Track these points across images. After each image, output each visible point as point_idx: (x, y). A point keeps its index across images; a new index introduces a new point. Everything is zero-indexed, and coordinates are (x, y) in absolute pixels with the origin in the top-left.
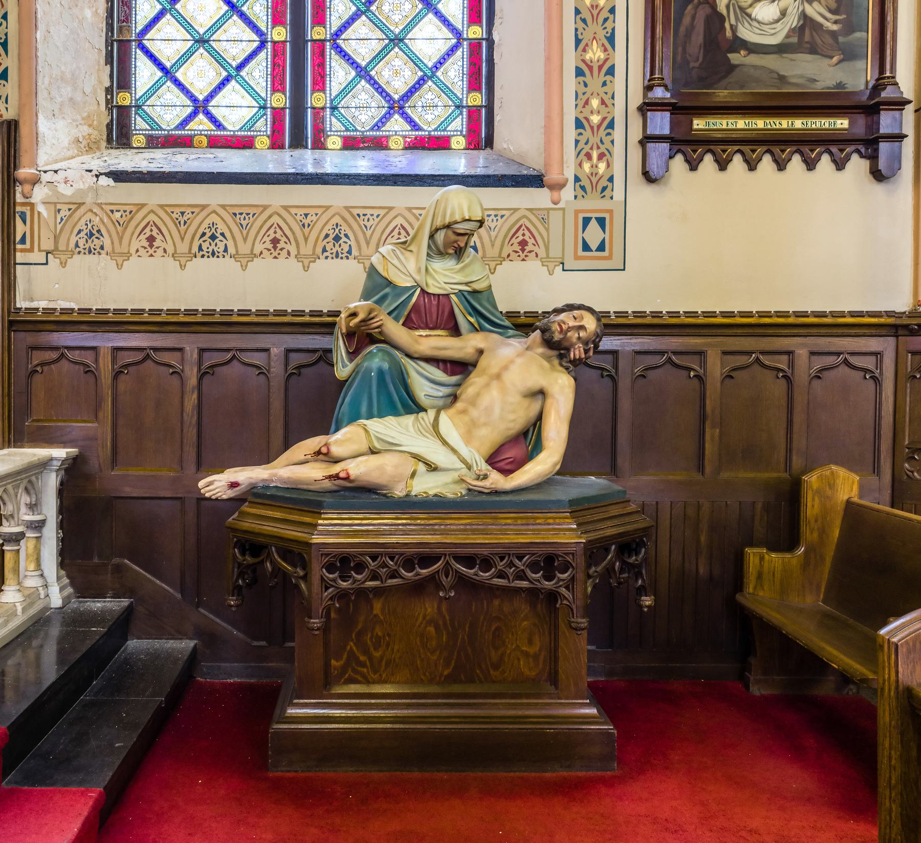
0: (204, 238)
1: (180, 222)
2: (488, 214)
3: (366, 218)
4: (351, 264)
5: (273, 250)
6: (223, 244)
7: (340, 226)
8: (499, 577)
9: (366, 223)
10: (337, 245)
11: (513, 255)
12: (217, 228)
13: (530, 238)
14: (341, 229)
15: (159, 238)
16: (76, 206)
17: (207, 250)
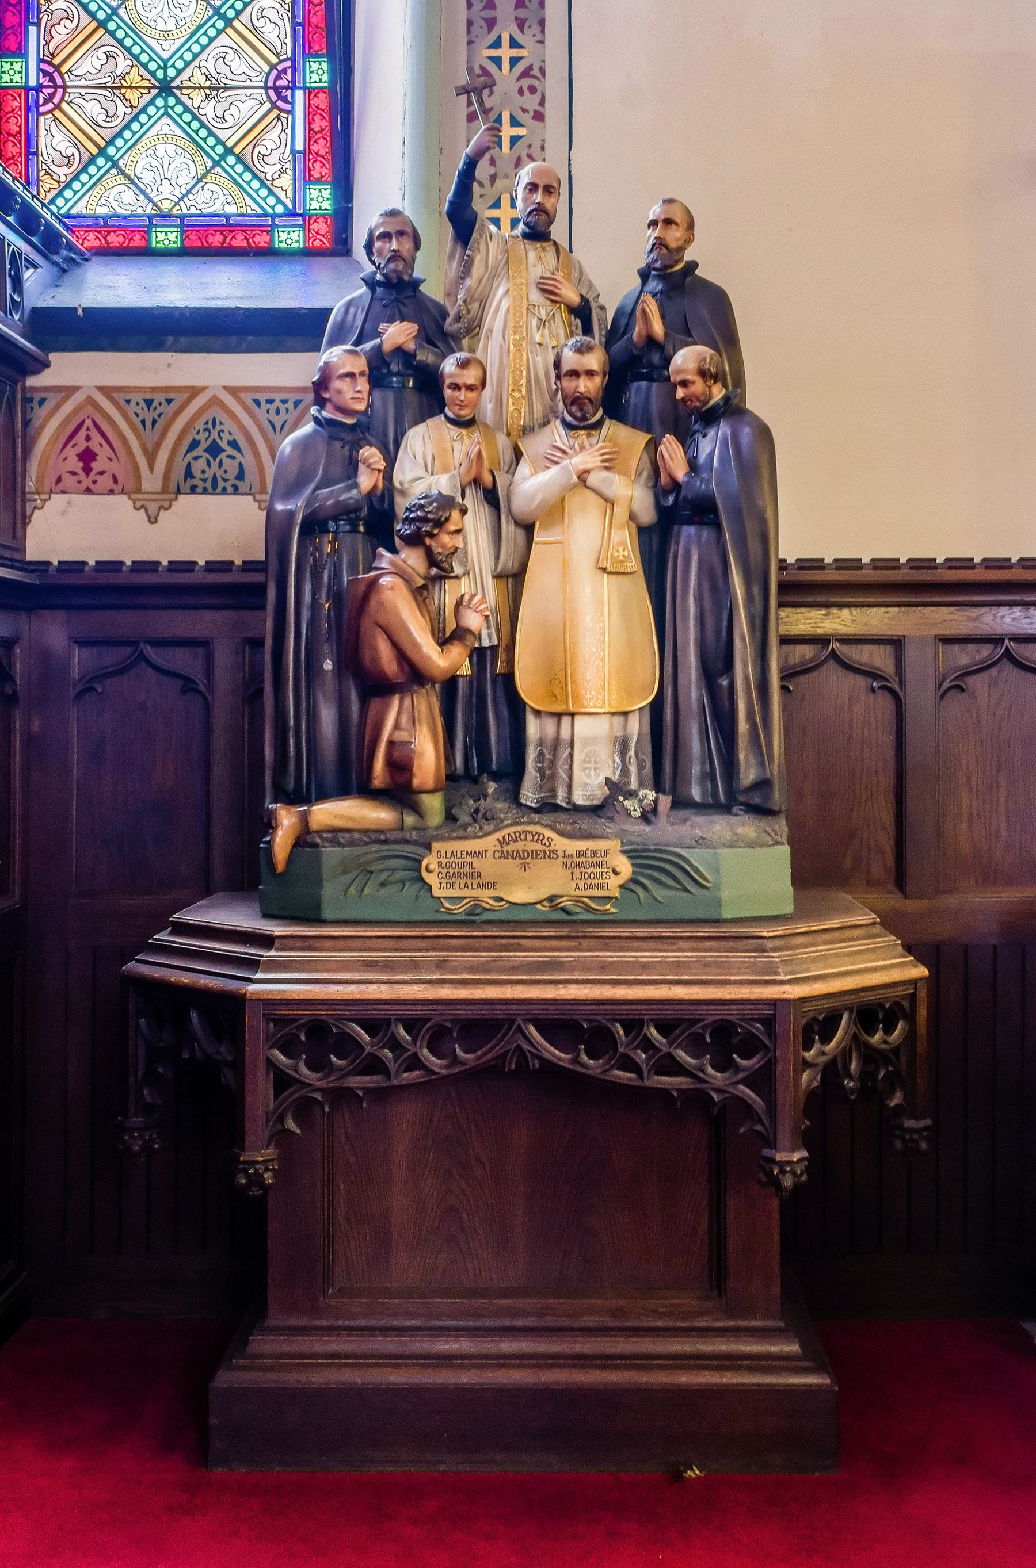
0: (195, 453)
1: (143, 422)
2: (284, 398)
3: (273, 407)
4: (246, 503)
5: (82, 475)
6: (236, 463)
7: (221, 423)
8: (621, 1068)
9: (272, 416)
10: (215, 464)
11: (69, 481)
12: (223, 431)
13: (101, 445)
14: (223, 431)
15: (103, 452)
16: (243, 395)
17: (202, 476)
